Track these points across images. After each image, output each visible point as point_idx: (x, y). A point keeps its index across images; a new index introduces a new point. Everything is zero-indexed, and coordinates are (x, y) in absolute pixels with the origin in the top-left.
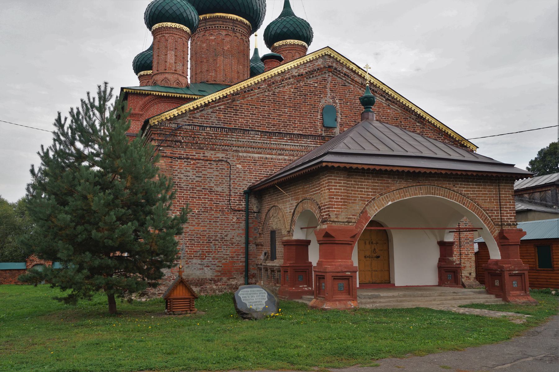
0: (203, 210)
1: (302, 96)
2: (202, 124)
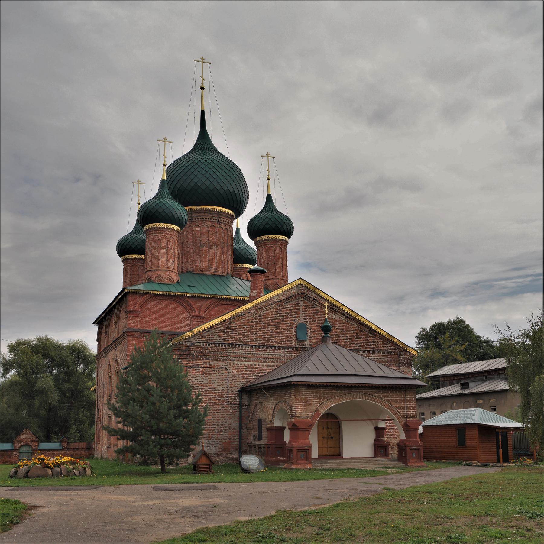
0: (209, 404)
1: (281, 317)
2: (208, 341)
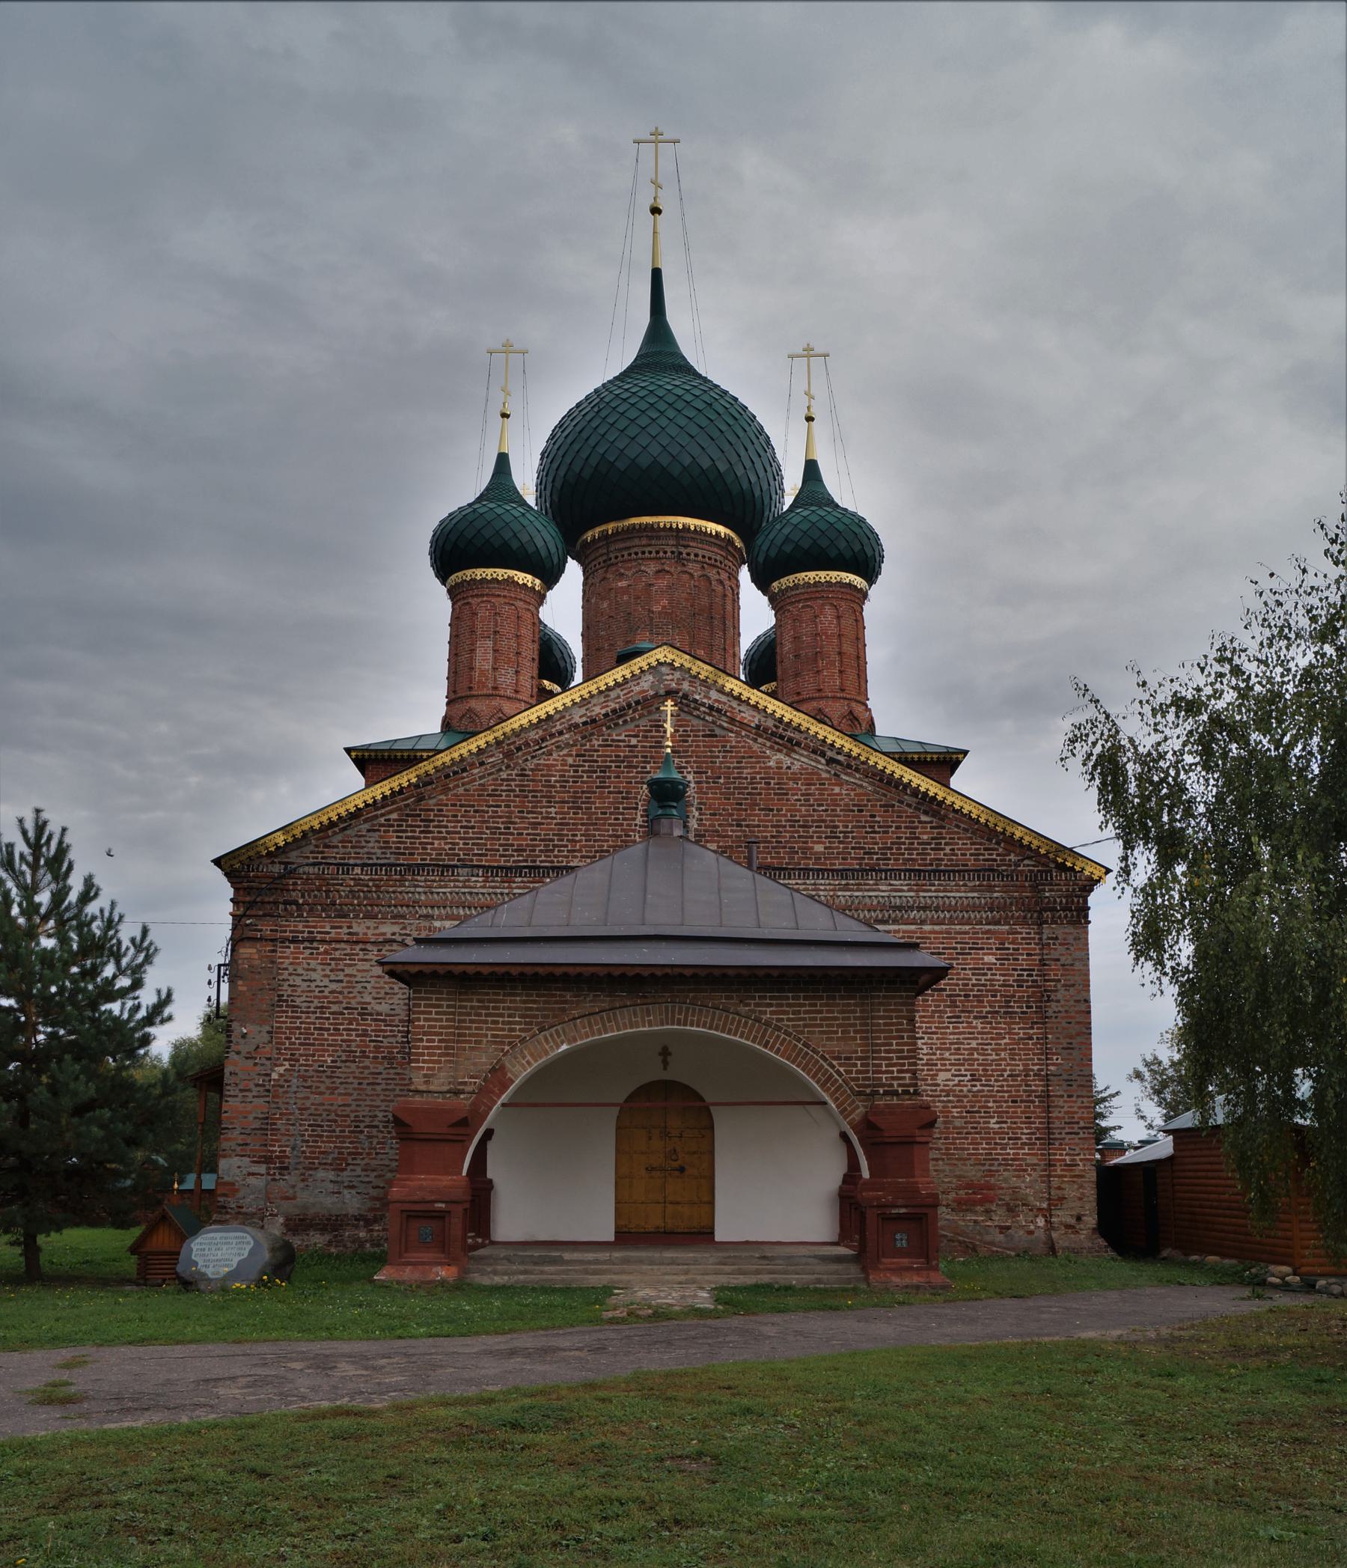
1: (596, 772)
2: (344, 859)
